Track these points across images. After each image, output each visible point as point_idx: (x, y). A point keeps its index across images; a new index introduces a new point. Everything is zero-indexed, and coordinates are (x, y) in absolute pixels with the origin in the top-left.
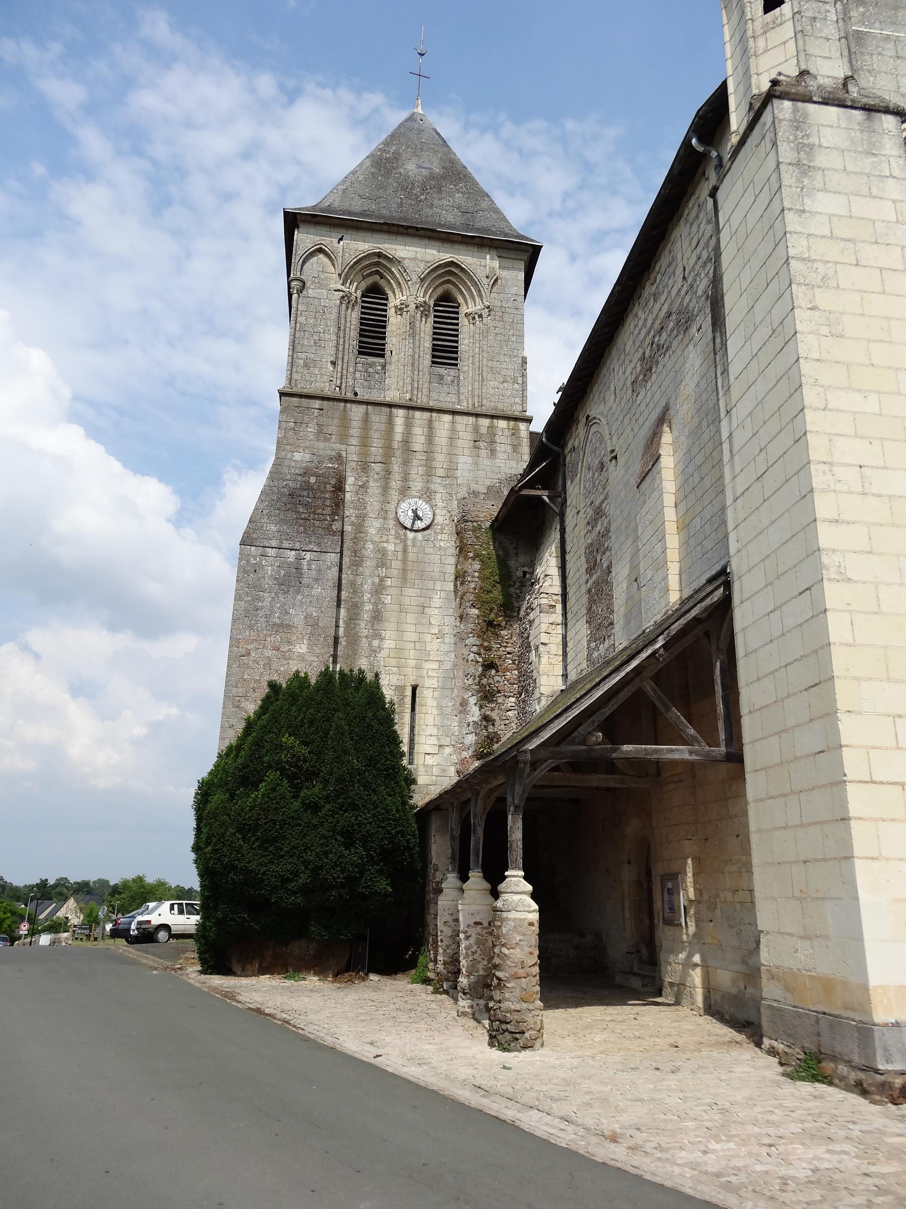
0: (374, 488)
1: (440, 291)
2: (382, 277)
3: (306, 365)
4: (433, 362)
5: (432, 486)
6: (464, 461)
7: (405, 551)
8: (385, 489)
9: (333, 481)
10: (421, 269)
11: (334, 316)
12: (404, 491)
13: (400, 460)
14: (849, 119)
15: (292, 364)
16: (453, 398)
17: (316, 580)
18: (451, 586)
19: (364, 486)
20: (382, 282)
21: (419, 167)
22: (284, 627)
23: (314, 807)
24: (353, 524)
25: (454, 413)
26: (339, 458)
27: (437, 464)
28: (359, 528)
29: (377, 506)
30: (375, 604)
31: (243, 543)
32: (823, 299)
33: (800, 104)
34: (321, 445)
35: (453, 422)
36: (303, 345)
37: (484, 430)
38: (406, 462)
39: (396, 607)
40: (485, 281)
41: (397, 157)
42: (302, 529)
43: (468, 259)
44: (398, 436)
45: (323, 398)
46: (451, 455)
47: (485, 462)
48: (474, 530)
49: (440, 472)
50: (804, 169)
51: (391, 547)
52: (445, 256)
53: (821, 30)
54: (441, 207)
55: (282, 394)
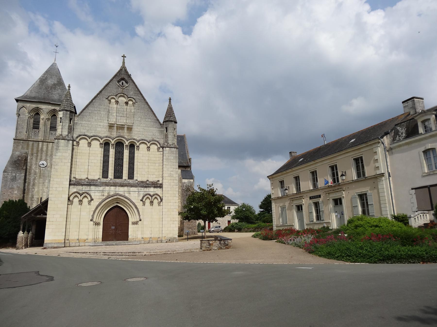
0: (34, 159)
1: (52, 114)
7: (40, 172)
8: (37, 159)
10: (47, 111)
11: (26, 121)
12: (41, 160)
15: (16, 133)
22: (12, 188)
23: (9, 222)
28: (31, 167)
32: (56, 167)
38: (42, 153)
41: (46, 79)
50: (57, 149)
51: (37, 171)
52: (53, 108)
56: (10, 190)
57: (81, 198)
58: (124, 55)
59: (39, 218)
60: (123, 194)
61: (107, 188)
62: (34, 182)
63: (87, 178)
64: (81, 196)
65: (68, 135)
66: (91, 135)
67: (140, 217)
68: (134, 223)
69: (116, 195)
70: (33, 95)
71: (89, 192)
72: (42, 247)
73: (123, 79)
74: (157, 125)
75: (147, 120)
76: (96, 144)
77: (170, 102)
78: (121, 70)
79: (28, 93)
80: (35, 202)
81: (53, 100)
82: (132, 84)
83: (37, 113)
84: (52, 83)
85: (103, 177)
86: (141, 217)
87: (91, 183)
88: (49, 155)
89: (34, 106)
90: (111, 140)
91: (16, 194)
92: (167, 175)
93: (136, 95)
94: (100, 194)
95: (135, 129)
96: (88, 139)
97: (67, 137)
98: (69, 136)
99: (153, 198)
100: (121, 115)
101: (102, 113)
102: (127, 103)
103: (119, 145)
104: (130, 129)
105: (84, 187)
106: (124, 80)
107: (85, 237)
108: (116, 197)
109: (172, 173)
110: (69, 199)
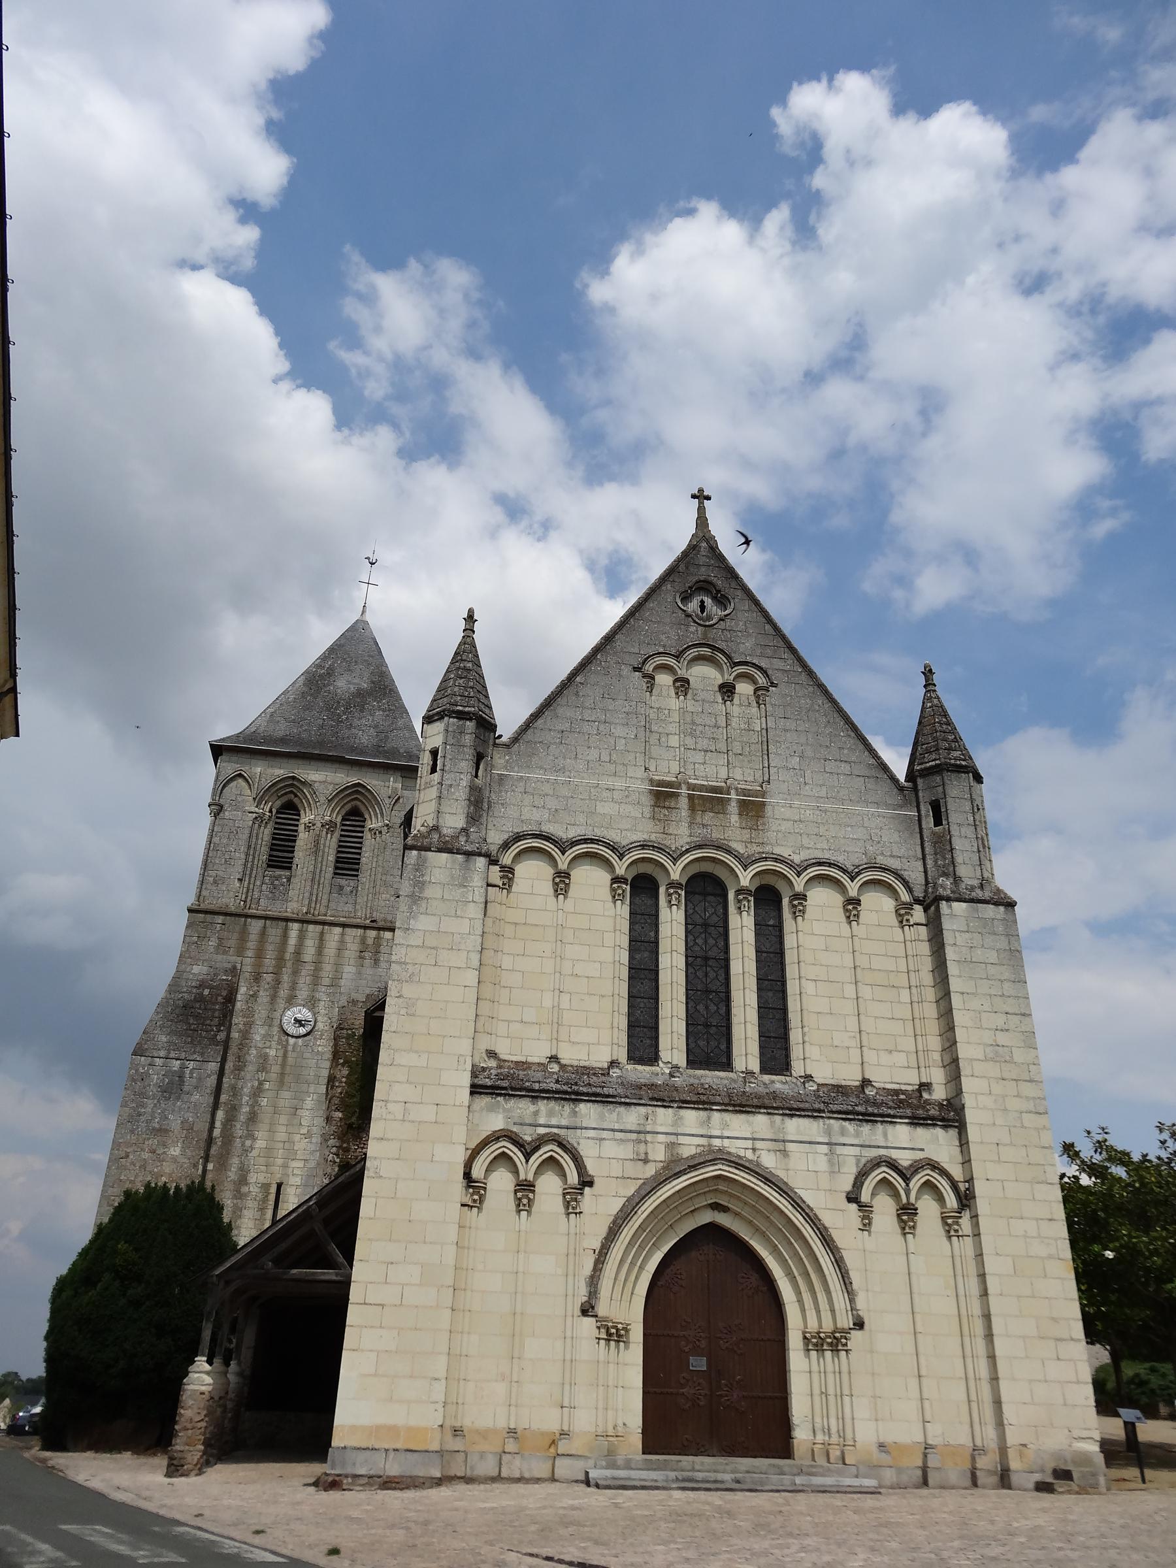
2: (296, 796)
3: (215, 882)
4: (335, 874)
5: (317, 995)
6: (349, 970)
7: (285, 1056)
8: (274, 998)
9: (224, 993)
10: (329, 791)
11: (246, 836)
12: (291, 1001)
13: (290, 971)
14: (454, 862)
15: (202, 882)
16: (350, 907)
17: (196, 1087)
18: (323, 1089)
19: (254, 996)
20: (296, 800)
21: (349, 682)
22: (162, 1131)
24: (240, 1031)
25: (344, 926)
26: (234, 971)
27: (324, 974)
28: (246, 1034)
29: (264, 1013)
30: (252, 1106)
31: (135, 1053)
32: (408, 990)
33: (423, 853)
34: (220, 957)
35: (343, 934)
36: (214, 864)
37: (370, 941)
38: (296, 973)
39: (271, 1109)
40: (387, 801)
41: (330, 672)
42: (189, 1039)
43: (374, 782)
44: (291, 949)
45: (226, 914)
46: (338, 966)
47: (369, 971)
48: (348, 1037)
49: (326, 981)
50: (415, 899)
51: (272, 1053)
53: (454, 793)
54: (359, 728)
55: (190, 911)
56: (153, 1142)
57: (527, 1170)
58: (701, 490)
59: (297, 1281)
60: (749, 1155)
61: (664, 1117)
62: (254, 1105)
63: (554, 1058)
64: (527, 1156)
65: (464, 830)
66: (572, 833)
67: (852, 1301)
68: (817, 1343)
69: (713, 1162)
70: (281, 730)
71: (571, 1137)
72: (315, 1469)
73: (704, 587)
74: (883, 790)
75: (830, 766)
76: (591, 881)
77: (929, 684)
78: (692, 548)
79: (263, 723)
80: (250, 1203)
81: (353, 750)
82: (747, 604)
83: (288, 803)
84: (352, 688)
85: (633, 1058)
86: (861, 1303)
87: (577, 1087)
88: (326, 981)
89: (279, 771)
90: (668, 864)
91: (174, 1160)
92: (978, 1053)
93: (769, 652)
94: (627, 1151)
95: (779, 807)
96: (556, 853)
97: (462, 839)
98: (473, 837)
99: (916, 1182)
100: (703, 743)
101: (619, 731)
102: (727, 690)
103: (705, 889)
104: (753, 808)
105: (542, 1105)
106: (707, 591)
107: (551, 1422)
108: (710, 1171)
109: (1002, 1038)
110: (467, 1175)
